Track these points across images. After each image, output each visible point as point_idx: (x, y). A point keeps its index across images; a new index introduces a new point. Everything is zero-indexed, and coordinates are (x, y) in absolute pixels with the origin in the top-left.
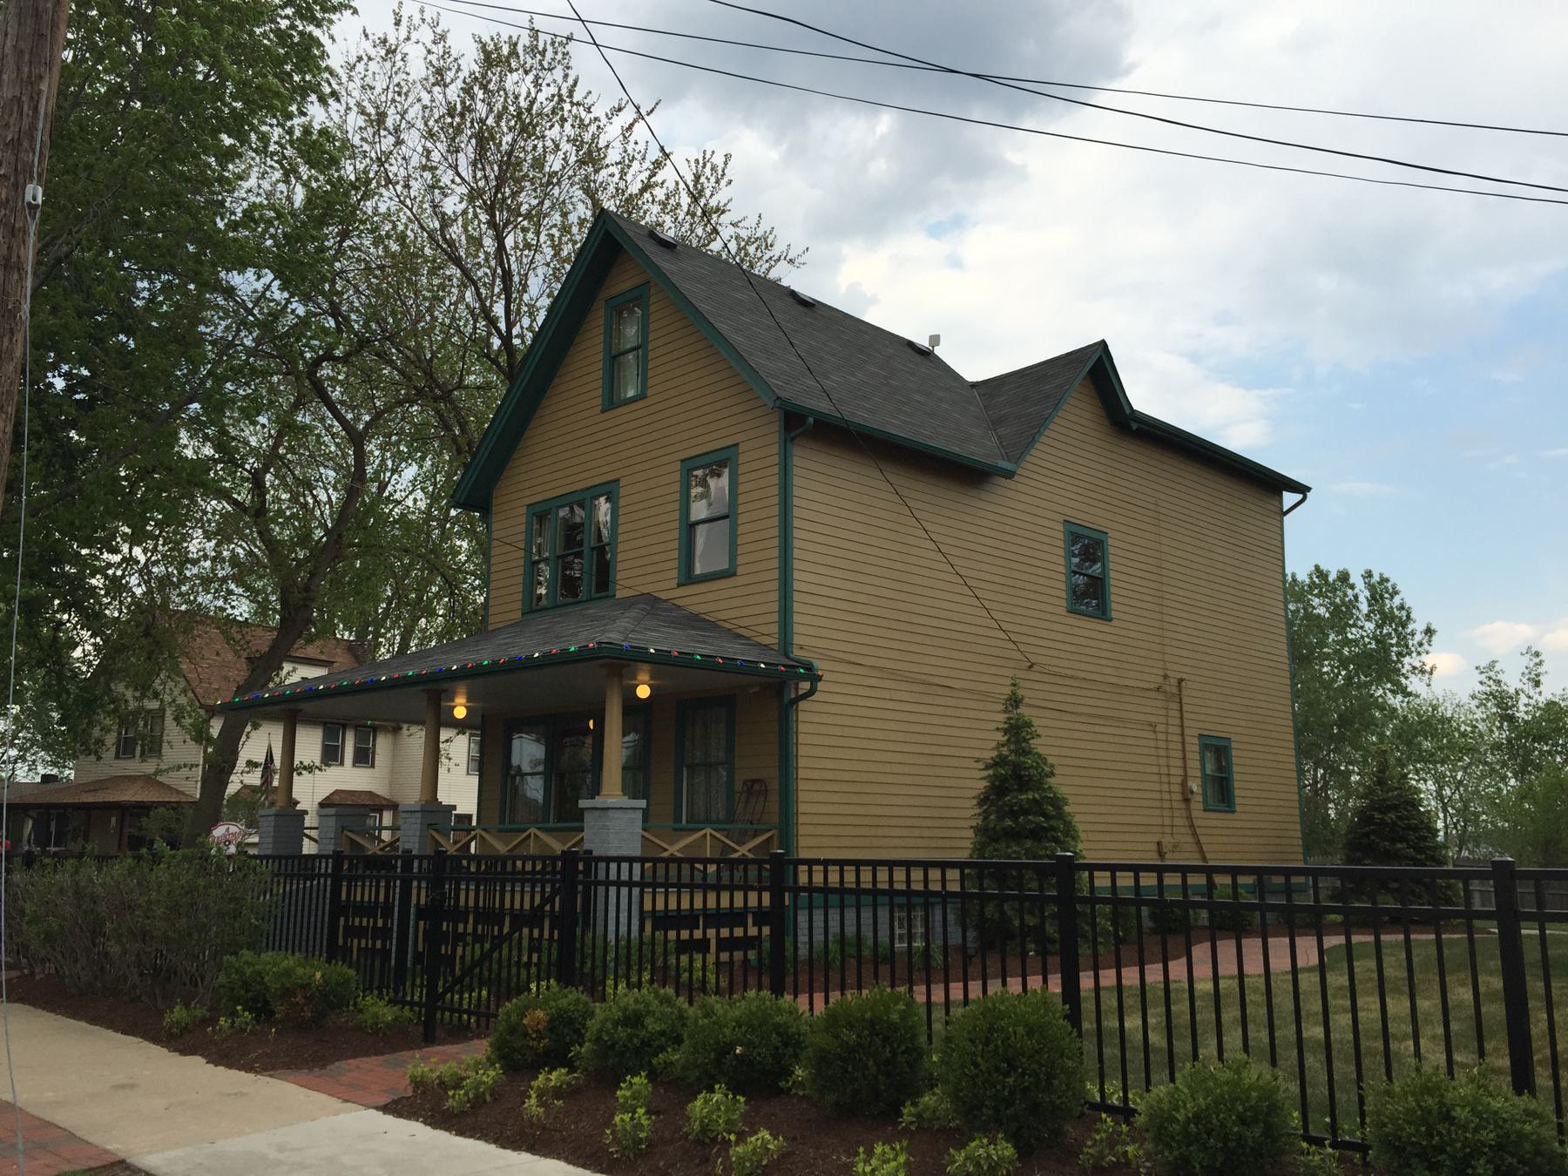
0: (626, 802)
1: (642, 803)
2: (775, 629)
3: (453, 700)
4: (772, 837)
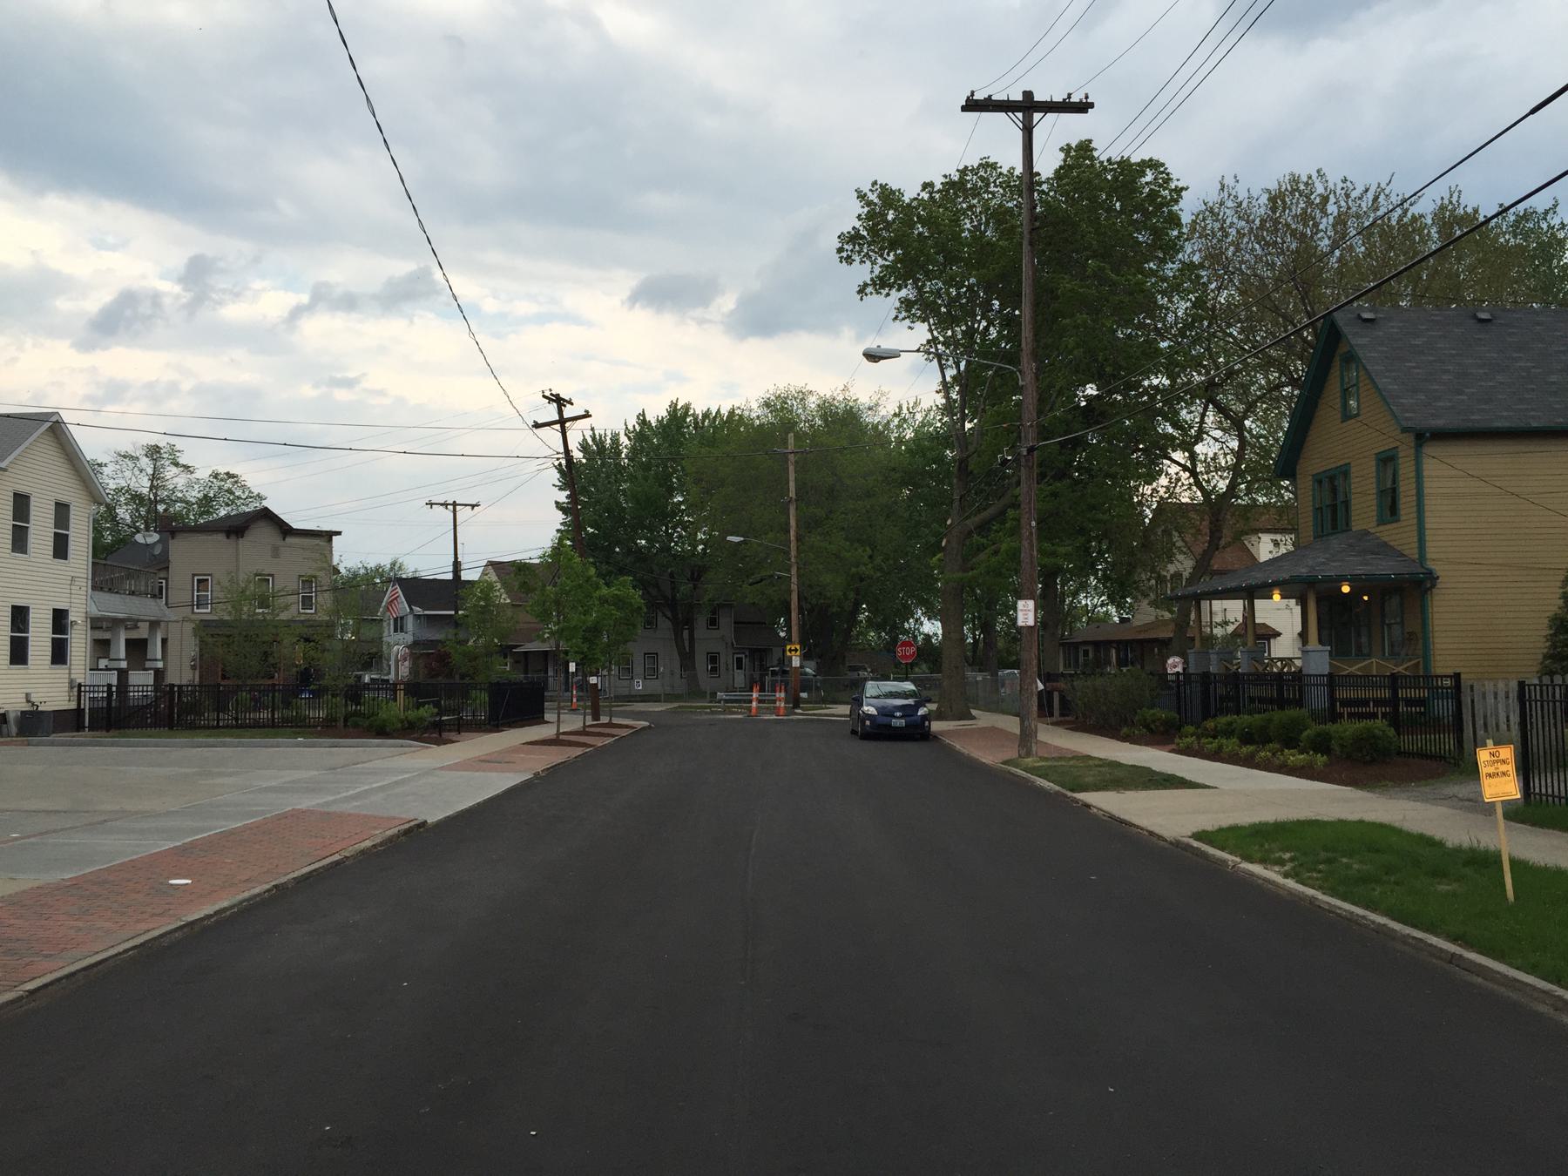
0: (1320, 647)
1: (1329, 648)
2: (1416, 551)
4: (1419, 662)
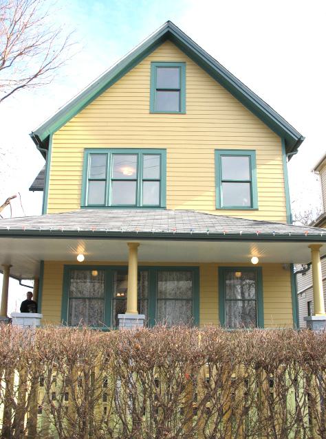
3: (250, 254)
